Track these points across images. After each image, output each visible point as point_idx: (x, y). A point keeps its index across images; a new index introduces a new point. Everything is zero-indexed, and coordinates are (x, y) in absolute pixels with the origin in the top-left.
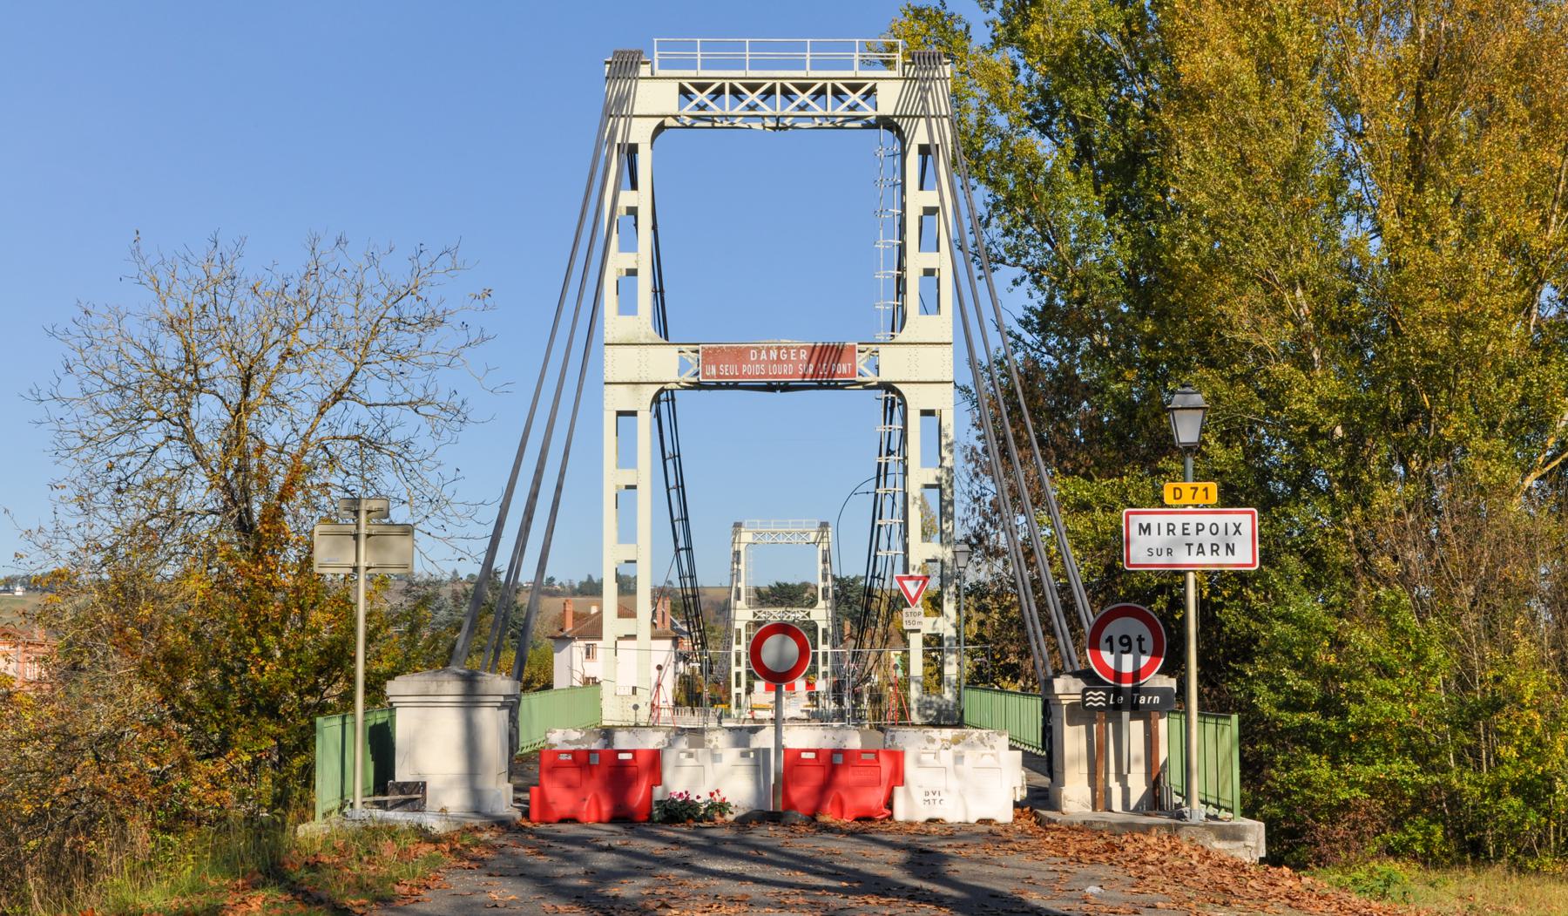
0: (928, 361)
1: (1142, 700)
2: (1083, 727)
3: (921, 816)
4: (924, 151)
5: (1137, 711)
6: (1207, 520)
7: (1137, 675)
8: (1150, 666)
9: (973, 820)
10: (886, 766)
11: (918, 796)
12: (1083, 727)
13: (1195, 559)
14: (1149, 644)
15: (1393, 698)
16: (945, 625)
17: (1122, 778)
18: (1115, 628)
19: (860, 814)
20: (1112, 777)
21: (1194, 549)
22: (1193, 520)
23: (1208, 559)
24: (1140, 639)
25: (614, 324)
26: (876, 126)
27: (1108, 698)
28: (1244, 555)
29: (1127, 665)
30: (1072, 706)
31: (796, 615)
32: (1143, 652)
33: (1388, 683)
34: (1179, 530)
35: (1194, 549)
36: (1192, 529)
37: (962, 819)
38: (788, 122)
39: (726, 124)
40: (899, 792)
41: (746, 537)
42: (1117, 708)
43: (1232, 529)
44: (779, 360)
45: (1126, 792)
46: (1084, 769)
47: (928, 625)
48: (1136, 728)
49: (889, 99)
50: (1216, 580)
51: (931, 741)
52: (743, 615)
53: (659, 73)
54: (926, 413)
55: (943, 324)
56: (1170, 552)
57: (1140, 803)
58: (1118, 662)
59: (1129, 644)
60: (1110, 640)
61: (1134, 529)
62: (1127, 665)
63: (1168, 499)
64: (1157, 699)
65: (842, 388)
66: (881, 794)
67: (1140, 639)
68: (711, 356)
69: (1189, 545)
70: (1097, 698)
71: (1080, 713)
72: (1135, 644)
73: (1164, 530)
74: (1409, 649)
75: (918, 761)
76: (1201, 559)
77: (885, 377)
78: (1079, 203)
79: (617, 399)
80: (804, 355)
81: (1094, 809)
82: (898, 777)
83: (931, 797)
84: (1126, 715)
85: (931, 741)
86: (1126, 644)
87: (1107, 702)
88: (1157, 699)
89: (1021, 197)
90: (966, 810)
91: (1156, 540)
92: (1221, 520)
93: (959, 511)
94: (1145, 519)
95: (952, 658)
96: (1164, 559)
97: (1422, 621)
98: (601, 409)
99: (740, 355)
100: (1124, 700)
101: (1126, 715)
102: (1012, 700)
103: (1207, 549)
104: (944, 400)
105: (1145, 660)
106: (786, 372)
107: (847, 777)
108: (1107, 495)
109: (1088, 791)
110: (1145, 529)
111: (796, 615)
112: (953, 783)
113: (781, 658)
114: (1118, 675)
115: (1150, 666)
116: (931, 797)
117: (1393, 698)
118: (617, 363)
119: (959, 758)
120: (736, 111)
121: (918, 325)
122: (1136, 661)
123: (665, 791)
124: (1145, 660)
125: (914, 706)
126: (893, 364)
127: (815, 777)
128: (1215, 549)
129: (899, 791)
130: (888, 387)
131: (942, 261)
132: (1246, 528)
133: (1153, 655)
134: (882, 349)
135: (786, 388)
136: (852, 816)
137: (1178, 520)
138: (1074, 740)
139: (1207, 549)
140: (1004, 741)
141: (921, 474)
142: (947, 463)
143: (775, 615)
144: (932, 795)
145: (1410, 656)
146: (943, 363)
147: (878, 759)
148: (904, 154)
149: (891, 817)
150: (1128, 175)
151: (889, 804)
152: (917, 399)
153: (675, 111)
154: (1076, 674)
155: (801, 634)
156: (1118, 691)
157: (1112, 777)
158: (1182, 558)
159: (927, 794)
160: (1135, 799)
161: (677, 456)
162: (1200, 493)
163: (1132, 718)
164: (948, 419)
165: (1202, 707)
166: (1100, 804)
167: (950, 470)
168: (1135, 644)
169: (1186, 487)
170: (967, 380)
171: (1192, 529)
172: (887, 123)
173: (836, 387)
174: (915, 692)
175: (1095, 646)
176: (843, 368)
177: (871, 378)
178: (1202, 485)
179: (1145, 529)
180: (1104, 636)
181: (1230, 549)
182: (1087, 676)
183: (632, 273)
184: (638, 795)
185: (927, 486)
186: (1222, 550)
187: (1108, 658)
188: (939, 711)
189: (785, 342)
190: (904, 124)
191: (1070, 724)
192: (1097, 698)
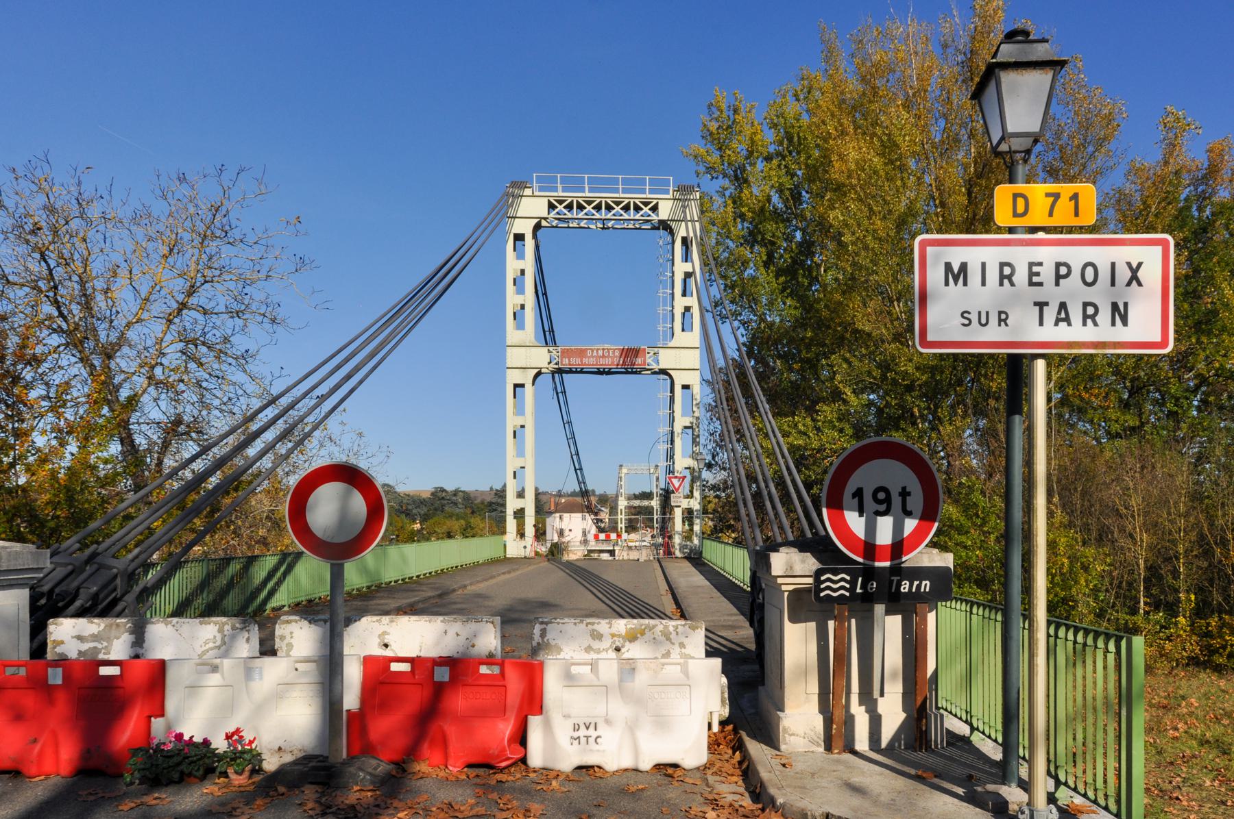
0: (685, 356)
1: (905, 587)
2: (812, 625)
3: (568, 758)
4: (685, 241)
5: (895, 602)
6: (1077, 256)
7: (898, 548)
8: (918, 535)
9: (646, 765)
10: (515, 684)
11: (563, 732)
12: (812, 625)
13: (1051, 332)
14: (916, 501)
15: (965, 547)
16: (695, 504)
17: (868, 699)
18: (868, 476)
19: (473, 760)
20: (855, 698)
21: (1050, 313)
22: (1048, 255)
23: (1077, 332)
24: (904, 494)
25: (512, 335)
26: (658, 228)
27: (853, 583)
28: (1147, 324)
29: (884, 533)
30: (797, 594)
31: (645, 503)
32: (909, 514)
33: (963, 538)
34: (1021, 276)
35: (1050, 313)
36: (1047, 274)
37: (627, 763)
38: (610, 225)
39: (575, 225)
40: (535, 724)
41: (624, 471)
42: (868, 599)
43: (1124, 274)
44: (603, 356)
45: (875, 722)
46: (814, 687)
47: (685, 504)
48: (891, 628)
49: (665, 212)
50: (1079, 373)
51: (597, 636)
52: (622, 504)
53: (537, 193)
54: (686, 387)
55: (694, 337)
56: (1003, 319)
57: (896, 738)
58: (871, 529)
59: (888, 500)
60: (859, 493)
61: (935, 275)
62: (884, 533)
63: (1002, 215)
64: (926, 585)
65: (640, 373)
66: (506, 729)
67: (904, 494)
68: (566, 353)
69: (1041, 305)
70: (838, 584)
71: (809, 604)
72: (896, 501)
73: (993, 275)
74: (978, 516)
75: (569, 679)
76: (1063, 333)
77: (662, 367)
78: (766, 282)
79: (513, 377)
80: (617, 353)
81: (829, 748)
82: (533, 702)
83: (583, 732)
84: (879, 609)
85: (597, 636)
86: (883, 502)
87: (852, 590)
88: (926, 585)
89: (742, 293)
90: (636, 752)
91: (979, 296)
92: (1102, 256)
93: (702, 440)
94: (956, 256)
95: (698, 521)
96: (993, 333)
97: (153, 565)
98: (505, 382)
99: (581, 353)
100: (879, 585)
101: (879, 609)
102: (729, 549)
103: (1076, 314)
104: (694, 379)
105: (910, 525)
106: (607, 363)
107: (460, 701)
108: (785, 427)
109: (818, 722)
110: (958, 274)
111: (645, 503)
112: (620, 710)
113: (344, 517)
114: (870, 549)
115: (918, 535)
116: (583, 732)
117: (965, 547)
118: (514, 357)
119: (629, 669)
120: (580, 216)
121: (681, 338)
122: (898, 527)
123: (169, 729)
124: (910, 525)
125: (677, 547)
126: (666, 359)
127: (413, 700)
128: (1090, 314)
129: (534, 722)
130: (664, 372)
131: (692, 301)
132: (1152, 273)
133: (922, 519)
134: (661, 351)
135: (609, 373)
136: (460, 762)
137: (1021, 256)
138: (798, 643)
139: (1076, 314)
140: (697, 641)
141: (681, 421)
142: (697, 414)
143: (637, 503)
144: (585, 729)
145: (979, 521)
146: (694, 359)
147: (502, 674)
148: (673, 242)
149: (524, 760)
150: (795, 273)
151: (521, 738)
152: (680, 379)
153: (546, 215)
154: (802, 545)
155: (649, 511)
156: (869, 573)
157: (855, 698)
158: (1031, 330)
159: (576, 728)
160: (889, 730)
161: (569, 422)
162: (1064, 205)
163: (889, 612)
164: (696, 389)
165: (1060, 610)
166: (838, 743)
167: (698, 418)
168: (896, 501)
169: (1038, 192)
170: (708, 376)
171: (1047, 274)
172: (665, 225)
173: (635, 373)
174: (677, 540)
175: (836, 504)
176: (639, 361)
177: (655, 367)
178: (1066, 189)
179: (958, 274)
180: (851, 487)
181: (1120, 313)
182: (819, 546)
183: (523, 307)
184: (125, 735)
185: (686, 427)
186: (1104, 316)
187: (856, 523)
188: (691, 550)
189: (606, 346)
190: (673, 225)
191: (794, 620)
192: (838, 584)
